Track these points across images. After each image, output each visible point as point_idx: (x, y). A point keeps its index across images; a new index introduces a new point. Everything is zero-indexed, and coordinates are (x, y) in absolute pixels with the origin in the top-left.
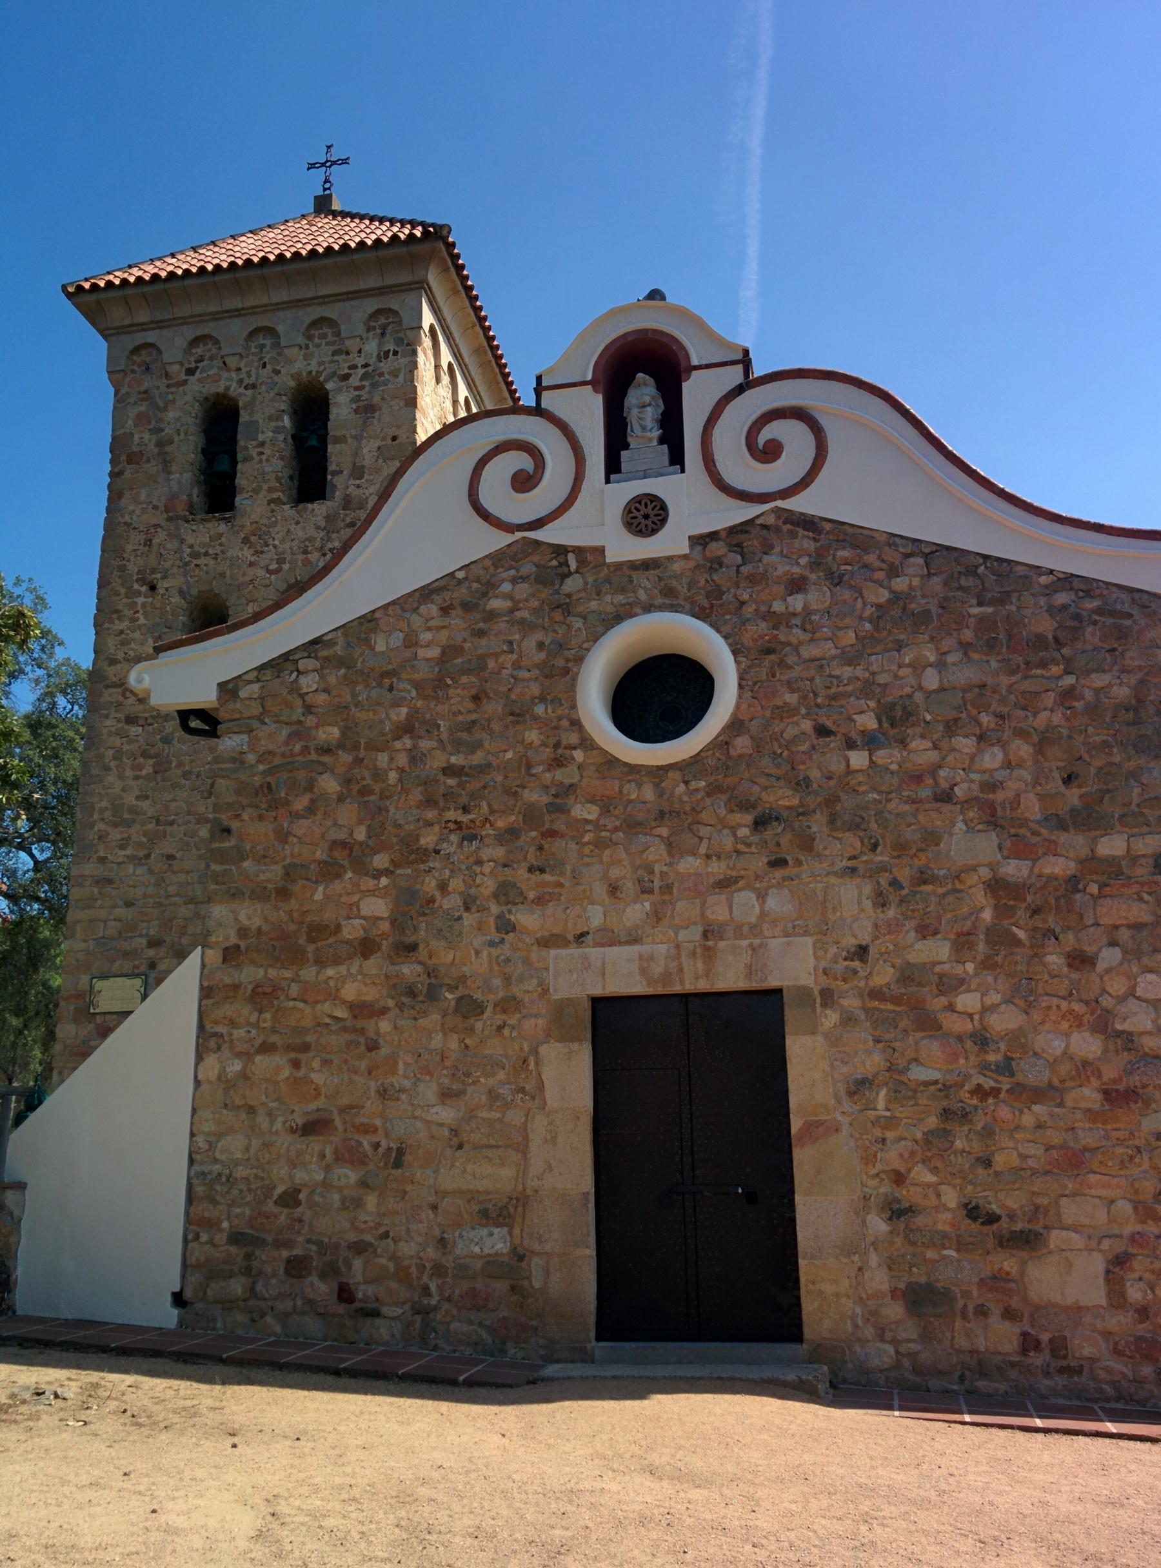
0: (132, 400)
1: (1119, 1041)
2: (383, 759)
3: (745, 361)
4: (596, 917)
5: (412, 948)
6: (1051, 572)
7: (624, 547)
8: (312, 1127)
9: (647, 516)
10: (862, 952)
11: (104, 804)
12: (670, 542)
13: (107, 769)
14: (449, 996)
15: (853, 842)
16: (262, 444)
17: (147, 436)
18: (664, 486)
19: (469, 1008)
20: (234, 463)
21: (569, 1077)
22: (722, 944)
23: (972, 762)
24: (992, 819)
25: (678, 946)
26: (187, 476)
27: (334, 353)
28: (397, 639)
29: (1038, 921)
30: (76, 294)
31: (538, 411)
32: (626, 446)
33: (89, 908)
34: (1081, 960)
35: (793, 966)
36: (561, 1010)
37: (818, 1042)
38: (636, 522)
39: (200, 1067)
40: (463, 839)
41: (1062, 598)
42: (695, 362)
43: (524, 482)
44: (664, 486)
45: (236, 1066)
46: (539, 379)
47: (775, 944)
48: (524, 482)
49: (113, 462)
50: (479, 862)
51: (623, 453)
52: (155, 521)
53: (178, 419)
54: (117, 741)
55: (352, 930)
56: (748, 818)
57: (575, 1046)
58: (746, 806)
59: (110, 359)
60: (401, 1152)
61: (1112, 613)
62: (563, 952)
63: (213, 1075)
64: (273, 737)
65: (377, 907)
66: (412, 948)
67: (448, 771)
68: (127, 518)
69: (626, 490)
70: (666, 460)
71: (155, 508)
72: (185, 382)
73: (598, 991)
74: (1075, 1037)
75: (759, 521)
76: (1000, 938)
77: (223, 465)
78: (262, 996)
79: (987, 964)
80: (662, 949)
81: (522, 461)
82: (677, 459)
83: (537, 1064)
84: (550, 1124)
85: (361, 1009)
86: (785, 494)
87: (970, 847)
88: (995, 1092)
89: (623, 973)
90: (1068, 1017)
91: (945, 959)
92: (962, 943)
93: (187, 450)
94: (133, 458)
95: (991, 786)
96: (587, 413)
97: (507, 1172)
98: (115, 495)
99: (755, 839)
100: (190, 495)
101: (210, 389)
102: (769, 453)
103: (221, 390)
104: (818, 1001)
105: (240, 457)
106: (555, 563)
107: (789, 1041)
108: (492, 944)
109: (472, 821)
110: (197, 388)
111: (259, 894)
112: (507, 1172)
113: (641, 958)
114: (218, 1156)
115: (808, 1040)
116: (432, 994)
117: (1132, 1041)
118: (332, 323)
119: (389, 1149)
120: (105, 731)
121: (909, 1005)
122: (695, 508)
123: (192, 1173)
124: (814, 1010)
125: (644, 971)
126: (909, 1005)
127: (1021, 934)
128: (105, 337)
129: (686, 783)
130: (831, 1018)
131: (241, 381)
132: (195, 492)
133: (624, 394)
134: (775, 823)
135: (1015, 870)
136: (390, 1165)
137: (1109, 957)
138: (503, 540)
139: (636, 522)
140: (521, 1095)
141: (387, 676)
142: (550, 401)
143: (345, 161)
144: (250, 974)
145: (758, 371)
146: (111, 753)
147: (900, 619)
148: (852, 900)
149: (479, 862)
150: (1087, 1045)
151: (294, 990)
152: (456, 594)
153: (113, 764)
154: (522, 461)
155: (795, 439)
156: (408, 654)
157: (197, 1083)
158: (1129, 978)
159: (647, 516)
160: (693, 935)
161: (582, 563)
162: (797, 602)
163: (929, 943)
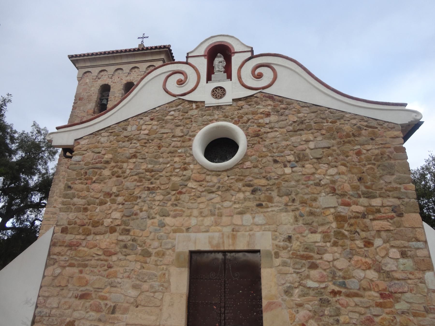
0: (82, 85)
1: (384, 274)
2: (125, 165)
3: (252, 51)
4: (193, 221)
5: (128, 231)
6: (350, 113)
7: (211, 101)
8: (84, 296)
9: (219, 92)
10: (289, 238)
11: (58, 191)
12: (227, 100)
13: (60, 181)
14: (139, 248)
15: (285, 199)
16: (115, 97)
17: (85, 94)
18: (226, 84)
19: (147, 254)
20: (108, 101)
21: (180, 281)
22: (239, 233)
23: (327, 173)
24: (333, 191)
25: (223, 234)
26: (94, 104)
27: (138, 75)
28: (134, 127)
29: (352, 228)
30: (71, 57)
31: (187, 63)
32: (214, 73)
33: (49, 221)
34: (368, 243)
35: (264, 242)
36: (179, 255)
37: (273, 271)
38: (215, 94)
39: (46, 271)
40: (150, 193)
41: (354, 122)
42: (236, 51)
43: (180, 83)
44: (226, 84)
45: (58, 271)
46: (188, 54)
47: (258, 234)
48: (180, 83)
49: (75, 100)
50: (154, 200)
51: (212, 75)
52: (84, 115)
53: (94, 90)
54: (64, 173)
55: (107, 222)
56: (250, 189)
57: (183, 269)
58: (249, 185)
59: (78, 74)
60: (115, 307)
61: (371, 127)
62: (181, 234)
63: (50, 273)
64: (90, 156)
65: (117, 215)
66: (128, 231)
67: (147, 170)
68: (76, 114)
69: (213, 85)
70: (226, 77)
71: (84, 112)
72: (97, 81)
73: (193, 249)
74: (368, 272)
75: (255, 96)
76: (338, 234)
77: (104, 102)
78: (71, 246)
79: (335, 244)
80: (217, 234)
81: (181, 77)
82: (229, 77)
83: (169, 276)
84: (172, 299)
85: (108, 253)
86: (264, 88)
87: (326, 200)
88: (339, 293)
89: (202, 242)
90: (365, 264)
91: (319, 241)
92: (326, 236)
93: (95, 97)
94: (80, 99)
95: (334, 182)
96: (202, 64)
97: (153, 318)
98: (74, 108)
99: (252, 196)
100: (94, 109)
101: (104, 83)
102: (259, 76)
103: (106, 83)
104: (274, 256)
105: (109, 100)
106: (188, 106)
107: (262, 270)
108: (156, 230)
109: (154, 187)
110: (101, 82)
111: (78, 210)
112: (153, 318)
113: (209, 237)
114: (47, 305)
115: (269, 270)
116: (133, 248)
117: (389, 274)
118: (137, 68)
119: (111, 306)
120: (61, 170)
121: (308, 258)
122: (234, 91)
123: (36, 312)
124: (272, 258)
125: (210, 242)
126: (308, 258)
127: (346, 233)
128: (78, 69)
129: (228, 176)
130: (277, 262)
131: (112, 81)
132: (96, 109)
133: (214, 59)
134: (259, 192)
135: (344, 211)
136: (110, 312)
137: (378, 242)
138: (174, 99)
139: (215, 94)
140: (162, 287)
141: (129, 139)
142: (190, 60)
143: (147, 37)
144: (68, 237)
145: (255, 54)
146: (61, 177)
147: (300, 127)
148: (286, 218)
149: (154, 200)
150: (372, 274)
151: (84, 243)
152: (156, 115)
153: (62, 180)
154: (181, 77)
155: (267, 73)
156: (138, 132)
157: (44, 276)
158: (386, 250)
159: (219, 92)
160: (227, 230)
161: (198, 107)
162: (267, 120)
163: (313, 235)
